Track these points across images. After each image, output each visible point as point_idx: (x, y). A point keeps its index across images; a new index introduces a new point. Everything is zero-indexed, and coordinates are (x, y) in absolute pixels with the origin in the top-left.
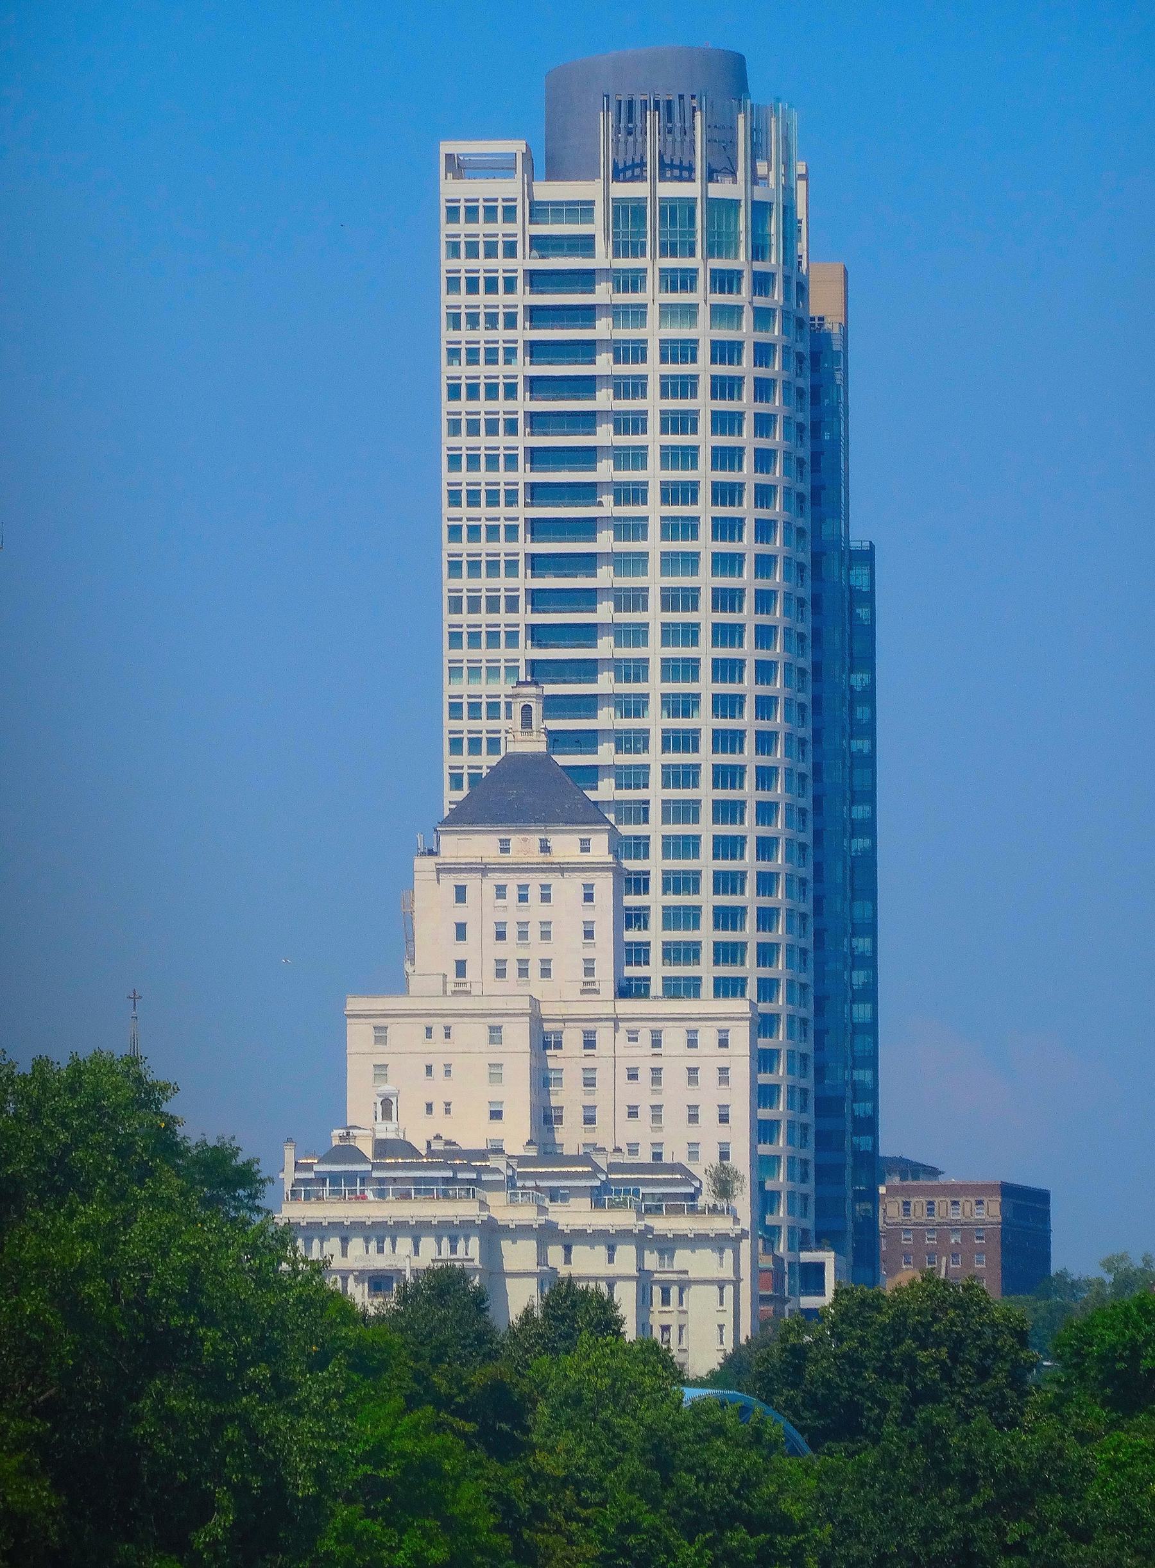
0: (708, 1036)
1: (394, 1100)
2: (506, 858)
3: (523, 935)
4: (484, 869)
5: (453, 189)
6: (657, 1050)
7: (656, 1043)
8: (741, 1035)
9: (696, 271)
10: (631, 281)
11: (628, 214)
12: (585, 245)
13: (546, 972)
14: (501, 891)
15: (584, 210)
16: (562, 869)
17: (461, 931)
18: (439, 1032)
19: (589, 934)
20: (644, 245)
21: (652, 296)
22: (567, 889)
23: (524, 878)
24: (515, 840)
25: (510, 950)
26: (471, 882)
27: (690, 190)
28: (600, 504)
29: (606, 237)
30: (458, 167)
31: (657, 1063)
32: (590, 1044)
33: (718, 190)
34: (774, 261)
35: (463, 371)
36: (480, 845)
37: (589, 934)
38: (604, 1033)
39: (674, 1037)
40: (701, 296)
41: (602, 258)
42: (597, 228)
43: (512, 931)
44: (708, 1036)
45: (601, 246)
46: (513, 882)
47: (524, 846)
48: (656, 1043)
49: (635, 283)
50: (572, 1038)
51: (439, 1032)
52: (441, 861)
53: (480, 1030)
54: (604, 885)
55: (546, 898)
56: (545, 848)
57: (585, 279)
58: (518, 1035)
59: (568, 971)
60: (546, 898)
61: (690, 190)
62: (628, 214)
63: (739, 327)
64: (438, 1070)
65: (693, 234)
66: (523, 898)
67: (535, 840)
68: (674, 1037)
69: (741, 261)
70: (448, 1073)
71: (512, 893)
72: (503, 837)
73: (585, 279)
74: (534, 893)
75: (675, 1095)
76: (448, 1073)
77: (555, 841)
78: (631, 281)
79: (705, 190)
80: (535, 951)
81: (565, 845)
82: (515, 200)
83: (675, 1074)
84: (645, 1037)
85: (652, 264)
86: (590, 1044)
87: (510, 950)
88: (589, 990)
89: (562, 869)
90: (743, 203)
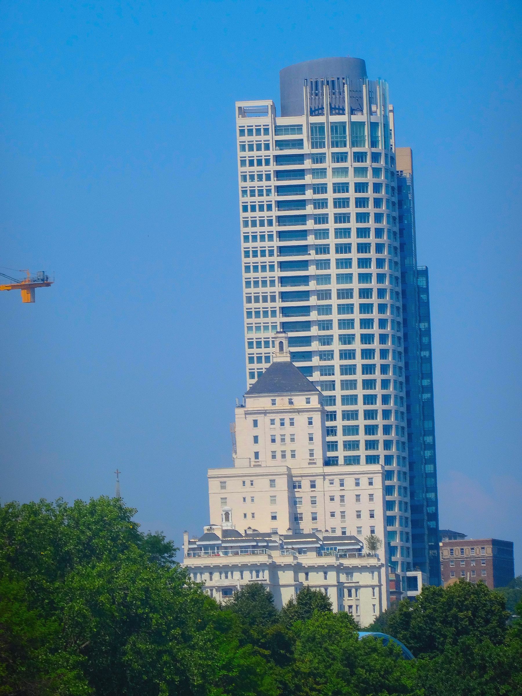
0: (364, 481)
1: (230, 513)
2: (308, 406)
3: (283, 440)
4: (265, 413)
5: (242, 122)
6: (342, 488)
7: (342, 485)
8: (378, 480)
9: (347, 153)
10: (319, 158)
11: (317, 130)
12: (299, 143)
13: (293, 456)
14: (273, 422)
15: (298, 128)
16: (299, 411)
17: (256, 439)
18: (248, 483)
19: (311, 439)
20: (324, 143)
21: (329, 164)
22: (301, 420)
23: (282, 416)
24: (278, 399)
25: (278, 447)
26: (260, 418)
27: (343, 118)
28: (310, 254)
29: (308, 140)
30: (243, 112)
31: (342, 493)
32: (313, 486)
33: (355, 118)
34: (380, 148)
35: (248, 199)
36: (263, 402)
37: (311, 439)
38: (319, 482)
39: (350, 482)
40: (350, 164)
41: (307, 149)
42: (304, 136)
43: (278, 439)
44: (364, 481)
45: (306, 144)
46: (277, 418)
47: (282, 402)
48: (342, 485)
49: (321, 159)
50: (306, 483)
51: (248, 483)
52: (246, 410)
53: (266, 481)
54: (317, 418)
55: (292, 424)
56: (291, 403)
57: (300, 158)
58: (282, 483)
59: (303, 455)
60: (292, 424)
61: (343, 118)
62: (317, 130)
63: (366, 177)
64: (248, 499)
65: (345, 137)
66: (282, 424)
67: (286, 399)
68: (350, 482)
69: (366, 148)
70: (253, 500)
71: (278, 422)
72: (290, 398)
73: (300, 158)
74: (287, 422)
75: (351, 506)
76: (253, 500)
77: (295, 399)
78: (319, 158)
79: (350, 118)
80: (289, 447)
81: (300, 401)
82: (268, 125)
83: (350, 497)
84: (337, 482)
85: (328, 151)
86: (313, 486)
87: (278, 447)
88: (312, 463)
89: (299, 411)
90: (366, 123)
